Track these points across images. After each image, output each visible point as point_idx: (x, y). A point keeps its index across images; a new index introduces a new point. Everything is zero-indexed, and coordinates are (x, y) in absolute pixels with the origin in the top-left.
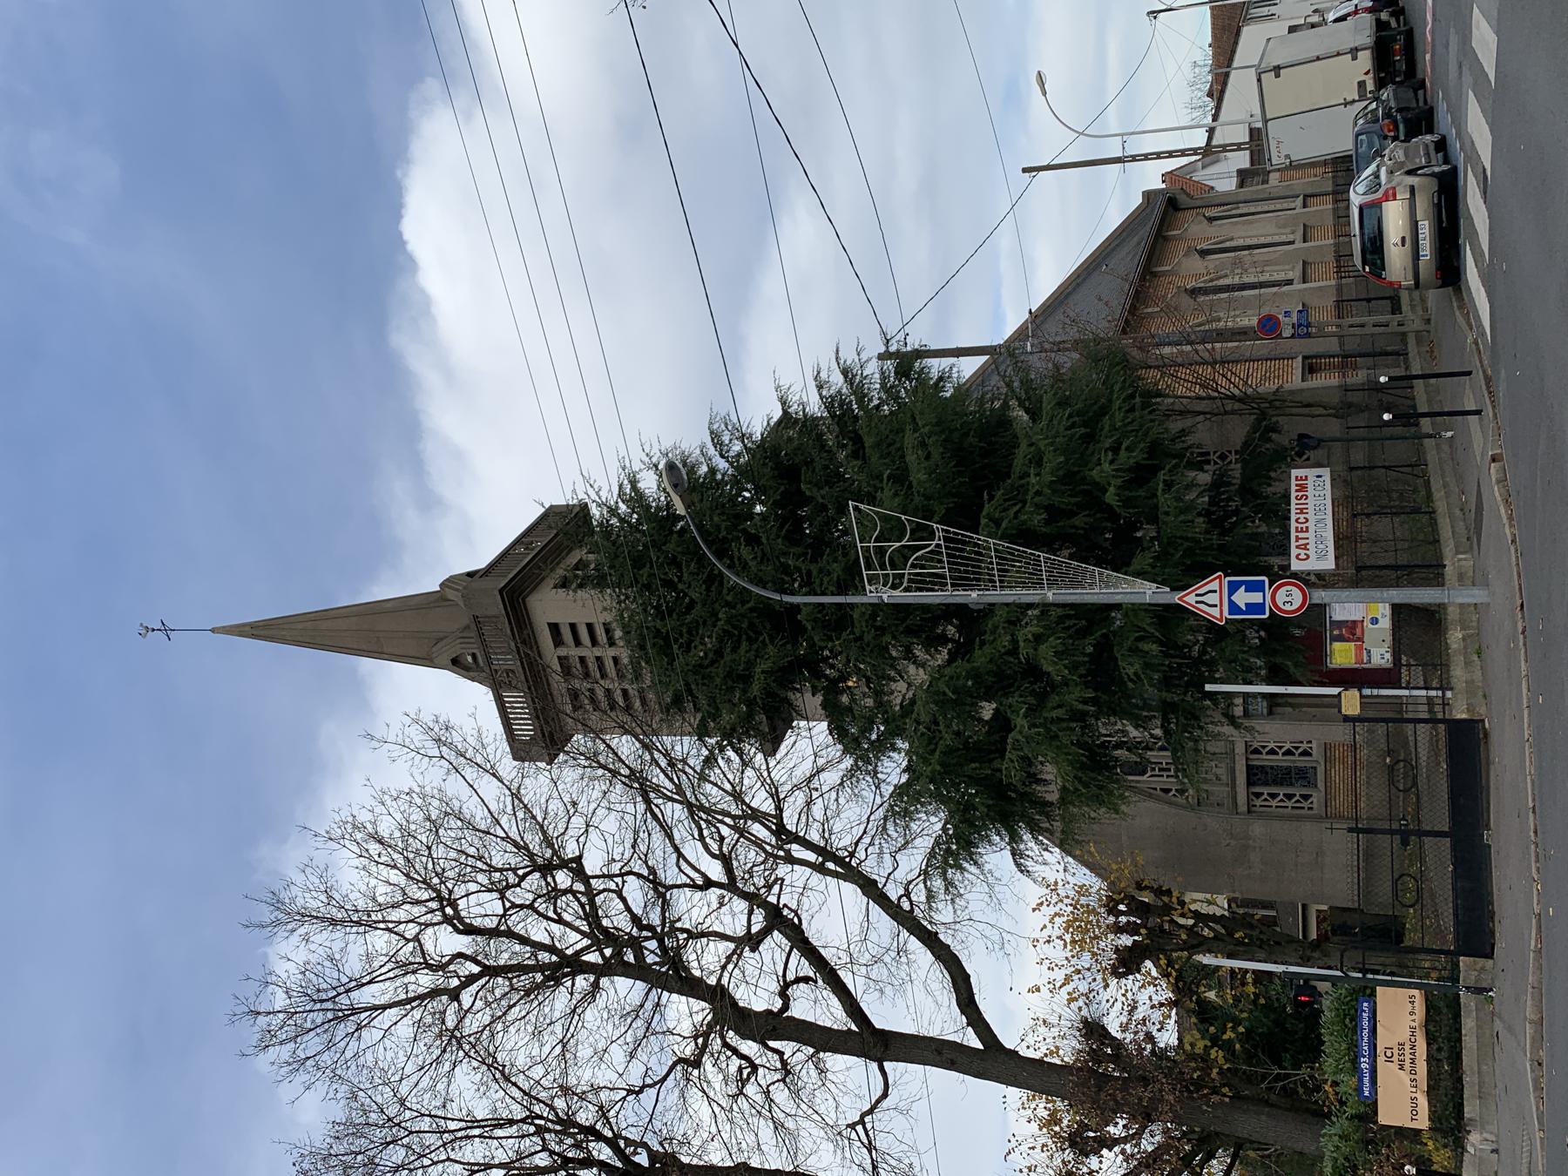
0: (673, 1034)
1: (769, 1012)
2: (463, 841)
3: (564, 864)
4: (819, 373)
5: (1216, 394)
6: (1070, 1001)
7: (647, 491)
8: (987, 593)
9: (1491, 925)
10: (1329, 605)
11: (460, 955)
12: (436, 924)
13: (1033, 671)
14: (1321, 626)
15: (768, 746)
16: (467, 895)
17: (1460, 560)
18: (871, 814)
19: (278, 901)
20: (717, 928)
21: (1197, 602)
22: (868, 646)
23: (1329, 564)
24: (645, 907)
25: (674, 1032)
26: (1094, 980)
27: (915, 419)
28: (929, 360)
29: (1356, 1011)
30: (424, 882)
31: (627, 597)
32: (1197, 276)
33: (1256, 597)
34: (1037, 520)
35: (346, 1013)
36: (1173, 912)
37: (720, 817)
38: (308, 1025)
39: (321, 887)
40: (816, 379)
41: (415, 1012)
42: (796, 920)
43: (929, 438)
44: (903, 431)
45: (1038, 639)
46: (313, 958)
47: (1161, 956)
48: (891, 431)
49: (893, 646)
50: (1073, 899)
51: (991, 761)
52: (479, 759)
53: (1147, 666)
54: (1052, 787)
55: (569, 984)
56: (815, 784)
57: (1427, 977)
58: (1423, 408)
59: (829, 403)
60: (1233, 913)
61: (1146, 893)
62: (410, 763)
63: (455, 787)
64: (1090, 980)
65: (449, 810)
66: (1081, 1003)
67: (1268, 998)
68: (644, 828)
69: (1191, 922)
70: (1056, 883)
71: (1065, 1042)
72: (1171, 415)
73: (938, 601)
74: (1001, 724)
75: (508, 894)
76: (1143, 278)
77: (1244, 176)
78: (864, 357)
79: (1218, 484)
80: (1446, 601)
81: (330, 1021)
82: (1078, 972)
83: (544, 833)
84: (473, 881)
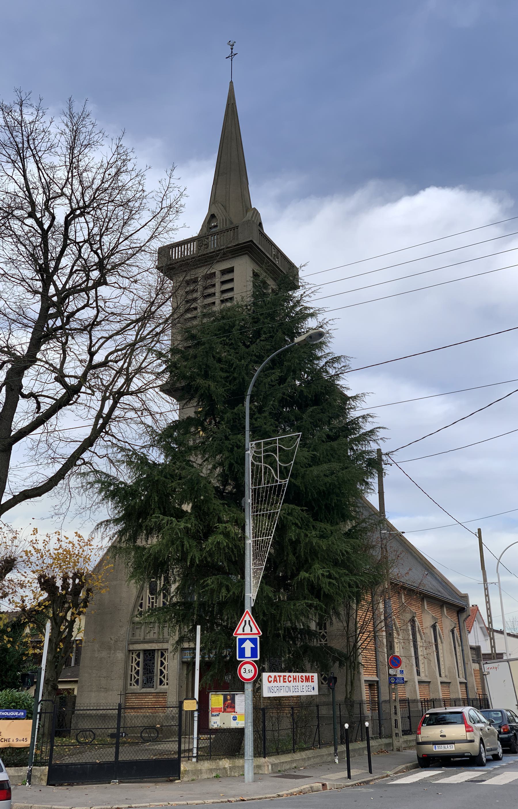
0: (9, 335)
1: (21, 387)
2: (116, 220)
3: (103, 275)
4: (371, 417)
5: (358, 633)
6: (26, 552)
7: (307, 322)
8: (251, 508)
9: (66, 784)
10: (244, 694)
11: (53, 218)
12: (71, 205)
13: (209, 532)
14: (232, 689)
15: (166, 388)
16: (87, 222)
17: (268, 766)
18: (129, 444)
19: (84, 118)
20: (68, 359)
21: (245, 621)
22: (222, 443)
23: (266, 693)
24: (80, 320)
25: (11, 335)
26: (37, 565)
27: (346, 468)
28: (377, 478)
29: (19, 709)
30: (94, 198)
31: (249, 310)
32: (421, 622)
33: (248, 653)
34: (292, 535)
35: (22, 155)
36: (75, 608)
37: (127, 361)
38: (15, 134)
39: (92, 142)
40: (368, 415)
41: (22, 193)
42: (71, 402)
43: (335, 476)
44: (340, 462)
45: (227, 535)
46: (52, 137)
47: (50, 602)
48: (339, 456)
49: (221, 457)
50: (82, 554)
51: (159, 508)
52: (160, 229)
53: (212, 591)
54: (144, 543)
55: (37, 278)
56: (145, 413)
57: (37, 749)
58: (351, 746)
59: (355, 422)
60: (73, 642)
61: (85, 593)
62: (159, 191)
63: (146, 216)
64: (37, 563)
65: (133, 212)
66: (25, 557)
67: (25, 662)
68: (122, 319)
69: (69, 618)
70: (91, 545)
71: (3, 549)
72: (347, 608)
73: (246, 481)
74: (180, 514)
75: (87, 245)
76: (420, 593)
77: (476, 650)
78: (380, 442)
79: (308, 632)
80: (246, 758)
81: (17, 145)
82: (42, 557)
83: (120, 265)
84: (94, 225)
